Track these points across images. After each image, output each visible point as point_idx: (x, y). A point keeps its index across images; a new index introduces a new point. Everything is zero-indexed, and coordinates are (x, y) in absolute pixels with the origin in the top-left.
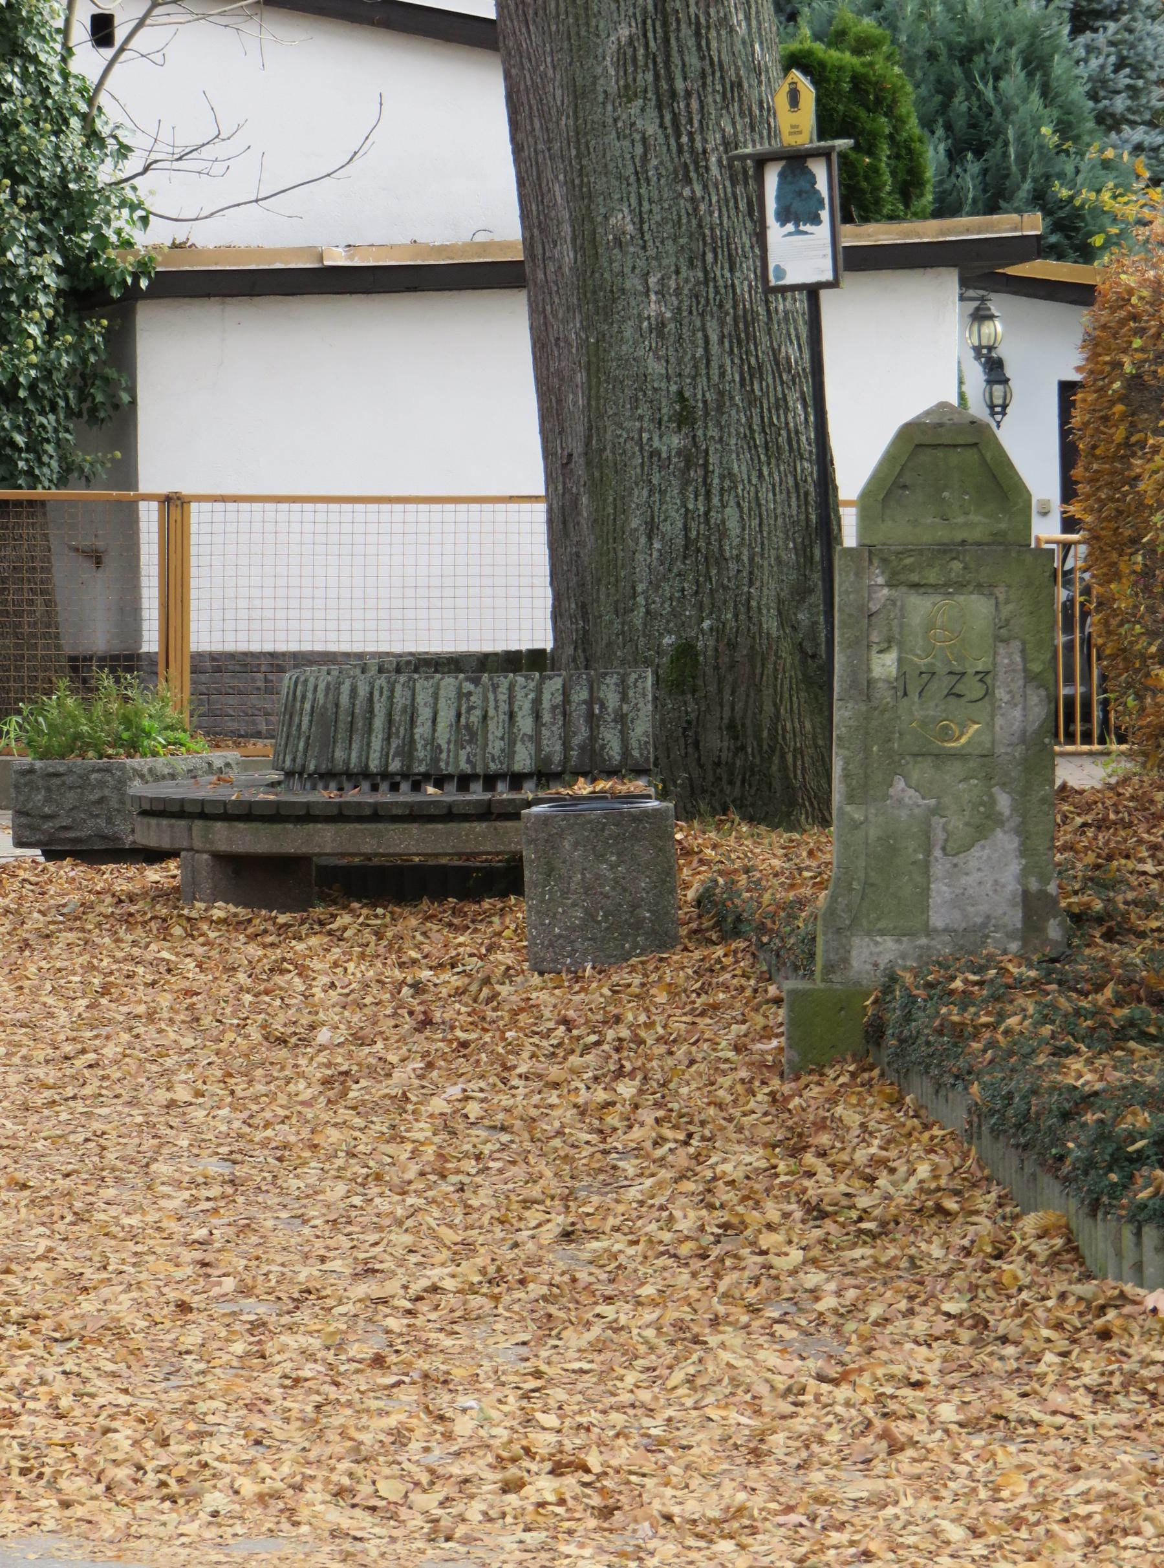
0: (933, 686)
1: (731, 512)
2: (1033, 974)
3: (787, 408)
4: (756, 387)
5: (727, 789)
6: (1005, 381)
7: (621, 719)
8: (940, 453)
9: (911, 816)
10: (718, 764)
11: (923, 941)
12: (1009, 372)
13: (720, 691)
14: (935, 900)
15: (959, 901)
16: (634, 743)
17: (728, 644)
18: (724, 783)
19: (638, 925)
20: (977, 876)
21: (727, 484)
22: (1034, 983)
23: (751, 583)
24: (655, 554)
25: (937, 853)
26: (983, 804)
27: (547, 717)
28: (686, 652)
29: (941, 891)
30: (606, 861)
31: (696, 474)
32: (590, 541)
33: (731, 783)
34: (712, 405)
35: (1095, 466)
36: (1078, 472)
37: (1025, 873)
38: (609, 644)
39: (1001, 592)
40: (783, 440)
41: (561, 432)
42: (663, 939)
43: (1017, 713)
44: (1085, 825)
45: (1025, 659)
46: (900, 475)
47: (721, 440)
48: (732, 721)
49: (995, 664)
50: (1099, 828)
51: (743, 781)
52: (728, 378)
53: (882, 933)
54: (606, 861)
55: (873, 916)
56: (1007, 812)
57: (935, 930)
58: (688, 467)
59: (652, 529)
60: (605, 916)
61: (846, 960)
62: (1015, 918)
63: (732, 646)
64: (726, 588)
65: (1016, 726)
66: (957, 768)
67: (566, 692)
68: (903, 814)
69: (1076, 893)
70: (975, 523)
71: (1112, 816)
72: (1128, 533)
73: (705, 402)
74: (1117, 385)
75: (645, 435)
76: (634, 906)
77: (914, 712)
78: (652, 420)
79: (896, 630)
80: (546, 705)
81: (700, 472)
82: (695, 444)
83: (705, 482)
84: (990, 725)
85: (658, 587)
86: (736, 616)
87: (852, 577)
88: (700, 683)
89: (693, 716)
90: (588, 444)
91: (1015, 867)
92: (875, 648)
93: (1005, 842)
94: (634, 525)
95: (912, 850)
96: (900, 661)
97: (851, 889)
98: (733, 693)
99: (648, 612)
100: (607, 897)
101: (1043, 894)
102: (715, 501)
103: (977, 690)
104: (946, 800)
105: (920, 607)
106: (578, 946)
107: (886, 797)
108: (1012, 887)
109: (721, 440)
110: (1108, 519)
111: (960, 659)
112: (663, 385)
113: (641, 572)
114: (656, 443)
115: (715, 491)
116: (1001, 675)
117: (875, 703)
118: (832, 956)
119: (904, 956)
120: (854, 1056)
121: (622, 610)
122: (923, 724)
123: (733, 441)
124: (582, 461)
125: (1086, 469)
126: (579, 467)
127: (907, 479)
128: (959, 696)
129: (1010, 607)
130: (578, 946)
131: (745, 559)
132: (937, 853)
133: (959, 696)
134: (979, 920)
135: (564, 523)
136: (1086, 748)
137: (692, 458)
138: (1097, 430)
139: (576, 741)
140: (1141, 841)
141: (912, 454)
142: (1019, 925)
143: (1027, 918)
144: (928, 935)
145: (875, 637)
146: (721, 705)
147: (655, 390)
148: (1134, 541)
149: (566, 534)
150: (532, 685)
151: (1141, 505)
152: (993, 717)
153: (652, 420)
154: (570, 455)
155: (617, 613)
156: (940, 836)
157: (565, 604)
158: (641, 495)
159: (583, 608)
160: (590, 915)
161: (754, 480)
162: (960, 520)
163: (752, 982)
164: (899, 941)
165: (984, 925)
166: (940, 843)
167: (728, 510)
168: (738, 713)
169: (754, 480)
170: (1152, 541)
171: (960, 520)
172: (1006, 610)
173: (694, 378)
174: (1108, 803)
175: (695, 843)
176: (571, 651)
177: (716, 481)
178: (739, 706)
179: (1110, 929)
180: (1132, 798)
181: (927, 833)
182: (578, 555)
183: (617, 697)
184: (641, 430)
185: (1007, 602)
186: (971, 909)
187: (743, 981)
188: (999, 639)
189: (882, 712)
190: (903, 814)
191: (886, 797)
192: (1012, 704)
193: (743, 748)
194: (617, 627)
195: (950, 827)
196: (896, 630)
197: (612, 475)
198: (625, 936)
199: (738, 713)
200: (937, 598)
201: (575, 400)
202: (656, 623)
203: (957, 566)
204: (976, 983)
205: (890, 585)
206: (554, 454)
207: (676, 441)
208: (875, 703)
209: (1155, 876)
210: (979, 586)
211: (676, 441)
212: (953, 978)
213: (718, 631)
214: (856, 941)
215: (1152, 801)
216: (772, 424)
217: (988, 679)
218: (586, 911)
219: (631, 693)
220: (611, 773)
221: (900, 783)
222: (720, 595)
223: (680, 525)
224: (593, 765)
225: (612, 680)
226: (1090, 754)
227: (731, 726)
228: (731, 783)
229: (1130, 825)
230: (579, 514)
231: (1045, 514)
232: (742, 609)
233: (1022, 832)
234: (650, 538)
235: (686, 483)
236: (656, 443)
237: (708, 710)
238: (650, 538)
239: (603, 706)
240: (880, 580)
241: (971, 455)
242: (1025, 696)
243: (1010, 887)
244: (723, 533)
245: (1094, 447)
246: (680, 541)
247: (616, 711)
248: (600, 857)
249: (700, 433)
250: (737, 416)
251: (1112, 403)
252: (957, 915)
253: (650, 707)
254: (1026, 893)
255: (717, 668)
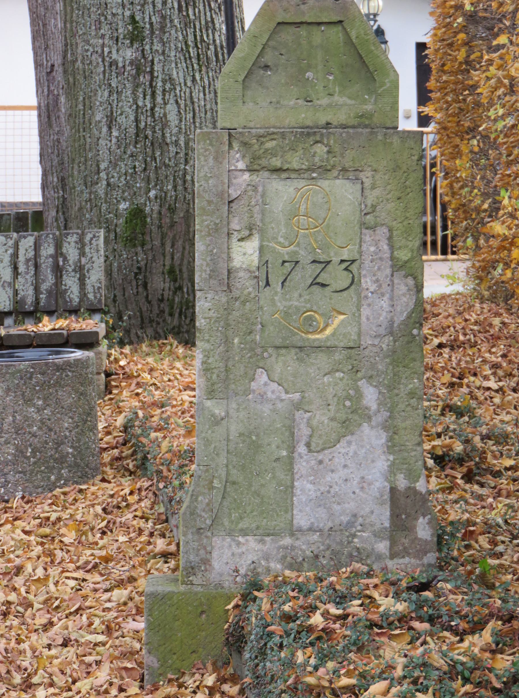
0: (296, 276)
1: (171, 108)
2: (401, 607)
3: (214, 29)
4: (191, 12)
5: (169, 319)
6: (386, 42)
7: (81, 271)
8: (303, 31)
9: (274, 410)
10: (161, 300)
11: (287, 541)
12: (387, 37)
13: (163, 244)
14: (299, 498)
15: (323, 500)
16: (89, 288)
17: (169, 209)
18: (166, 314)
19: (61, 460)
20: (342, 473)
21: (168, 86)
22: (403, 619)
23: (186, 162)
24: (114, 140)
25: (302, 449)
26: (348, 398)
27: (22, 268)
28: (137, 214)
29: (305, 488)
30: (34, 405)
31: (145, 79)
32: (67, 131)
33: (171, 315)
34: (156, 26)
35: (444, 78)
36: (431, 84)
37: (393, 469)
38: (80, 209)
39: (366, 177)
40: (211, 53)
41: (47, 48)
42: (84, 470)
43: (385, 303)
44: (441, 346)
45: (392, 247)
46: (261, 54)
47: (163, 53)
48: (172, 267)
49: (360, 253)
50: (452, 348)
51: (180, 314)
52: (169, 5)
53: (244, 533)
54: (34, 405)
55: (235, 515)
56: (374, 407)
57: (300, 530)
58: (138, 74)
59: (111, 121)
60: (34, 452)
61: (206, 562)
62: (383, 517)
63: (172, 210)
64: (167, 166)
65: (384, 317)
66: (322, 361)
67: (37, 247)
68: (266, 409)
69: (439, 435)
70: (339, 106)
71: (461, 338)
72: (467, 124)
73: (151, 24)
74: (460, 20)
75: (106, 50)
76: (58, 444)
77: (276, 302)
78: (111, 38)
79: (257, 217)
80: (22, 258)
81: (148, 77)
82: (144, 56)
83: (151, 85)
84: (357, 316)
85: (116, 165)
86: (175, 187)
87: (211, 161)
88: (148, 238)
89: (143, 263)
90: (65, 57)
91: (382, 463)
92: (236, 236)
93: (372, 437)
94: (98, 118)
95: (275, 447)
96: (261, 249)
97: (211, 488)
98: (173, 246)
99: (108, 184)
100: (34, 435)
101: (411, 491)
102: (159, 99)
103: (344, 280)
104: (310, 395)
105: (282, 193)
106: (10, 477)
107: (248, 391)
108: (379, 484)
109: (163, 53)
110: (453, 115)
111: (325, 247)
112: (120, 11)
113: (104, 154)
114: (114, 56)
115: (159, 92)
116: (367, 264)
117: (236, 293)
118: (192, 558)
119: (267, 557)
120: (214, 664)
121: (90, 183)
122: (287, 314)
123: (173, 54)
124: (61, 70)
125: (437, 81)
126: (59, 75)
127: (268, 58)
128: (323, 285)
129: (377, 192)
130: (10, 477)
131: (182, 143)
132: (302, 449)
133: (323, 285)
134: (345, 519)
135: (49, 117)
136: (434, 257)
137: (141, 67)
138: (445, 53)
139: (44, 287)
140: (485, 361)
141: (274, 32)
142: (387, 524)
143: (395, 516)
144: (292, 535)
145: (235, 225)
146: (164, 255)
147: (114, 15)
148: (473, 130)
149: (50, 126)
150: (11, 243)
151: (478, 104)
152: (359, 307)
153: (111, 38)
154: (53, 66)
155: (86, 184)
156: (305, 431)
157: (50, 178)
158: (103, 95)
159: (62, 180)
160: (20, 451)
161: (189, 84)
162: (325, 101)
163: (150, 524)
164: (262, 542)
165: (350, 524)
166: (305, 439)
167: (168, 107)
168: (177, 262)
169: (189, 84)
170: (486, 129)
171: (325, 101)
172: (372, 197)
173: (143, 6)
174: (458, 327)
175: (133, 368)
176: (54, 213)
177: (160, 84)
178: (177, 256)
179: (470, 471)
180: (476, 323)
181: (291, 430)
182: (58, 141)
183: (77, 252)
184: (103, 46)
185: (373, 188)
186: (336, 508)
187: (142, 523)
188: (364, 225)
189: (244, 303)
190: (266, 409)
191: (248, 391)
192: (379, 293)
193: (180, 288)
194: (86, 196)
195: (314, 423)
196: (257, 217)
197: (82, 80)
198: (50, 469)
199: (177, 262)
200: (301, 183)
201: (56, 24)
202: (115, 193)
203: (321, 149)
204: (339, 618)
205: (250, 170)
206: (42, 65)
207: (129, 54)
208: (236, 293)
209: (497, 391)
210: (344, 170)
211: (129, 54)
212: (313, 609)
213: (161, 199)
214: (217, 541)
215: (491, 325)
216: (202, 40)
217: (354, 268)
218: (17, 448)
219: (87, 249)
220: (74, 311)
221: (262, 377)
222: (163, 171)
223: (132, 118)
224: (57, 306)
225: (73, 239)
226: (437, 260)
227: (171, 271)
228: (171, 315)
229: (475, 344)
230: (59, 110)
231: (408, 117)
232: (180, 182)
233: (390, 428)
234: (110, 128)
235: (137, 86)
236: (114, 56)
237: (154, 259)
238: (110, 128)
239: (65, 259)
240: (241, 165)
241: (335, 34)
242: (392, 285)
243: (378, 484)
244: (165, 125)
245: (443, 65)
246: (132, 131)
247: (75, 264)
248: (28, 402)
249: (147, 47)
250: (175, 35)
251: (456, 33)
252: (322, 513)
253: (102, 259)
254: (393, 490)
255: (160, 227)
